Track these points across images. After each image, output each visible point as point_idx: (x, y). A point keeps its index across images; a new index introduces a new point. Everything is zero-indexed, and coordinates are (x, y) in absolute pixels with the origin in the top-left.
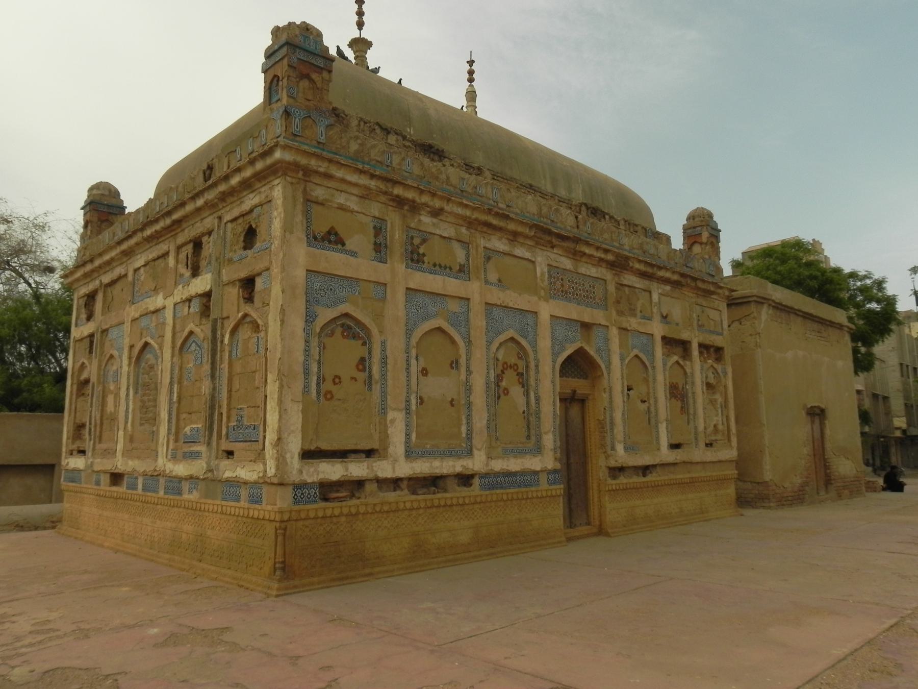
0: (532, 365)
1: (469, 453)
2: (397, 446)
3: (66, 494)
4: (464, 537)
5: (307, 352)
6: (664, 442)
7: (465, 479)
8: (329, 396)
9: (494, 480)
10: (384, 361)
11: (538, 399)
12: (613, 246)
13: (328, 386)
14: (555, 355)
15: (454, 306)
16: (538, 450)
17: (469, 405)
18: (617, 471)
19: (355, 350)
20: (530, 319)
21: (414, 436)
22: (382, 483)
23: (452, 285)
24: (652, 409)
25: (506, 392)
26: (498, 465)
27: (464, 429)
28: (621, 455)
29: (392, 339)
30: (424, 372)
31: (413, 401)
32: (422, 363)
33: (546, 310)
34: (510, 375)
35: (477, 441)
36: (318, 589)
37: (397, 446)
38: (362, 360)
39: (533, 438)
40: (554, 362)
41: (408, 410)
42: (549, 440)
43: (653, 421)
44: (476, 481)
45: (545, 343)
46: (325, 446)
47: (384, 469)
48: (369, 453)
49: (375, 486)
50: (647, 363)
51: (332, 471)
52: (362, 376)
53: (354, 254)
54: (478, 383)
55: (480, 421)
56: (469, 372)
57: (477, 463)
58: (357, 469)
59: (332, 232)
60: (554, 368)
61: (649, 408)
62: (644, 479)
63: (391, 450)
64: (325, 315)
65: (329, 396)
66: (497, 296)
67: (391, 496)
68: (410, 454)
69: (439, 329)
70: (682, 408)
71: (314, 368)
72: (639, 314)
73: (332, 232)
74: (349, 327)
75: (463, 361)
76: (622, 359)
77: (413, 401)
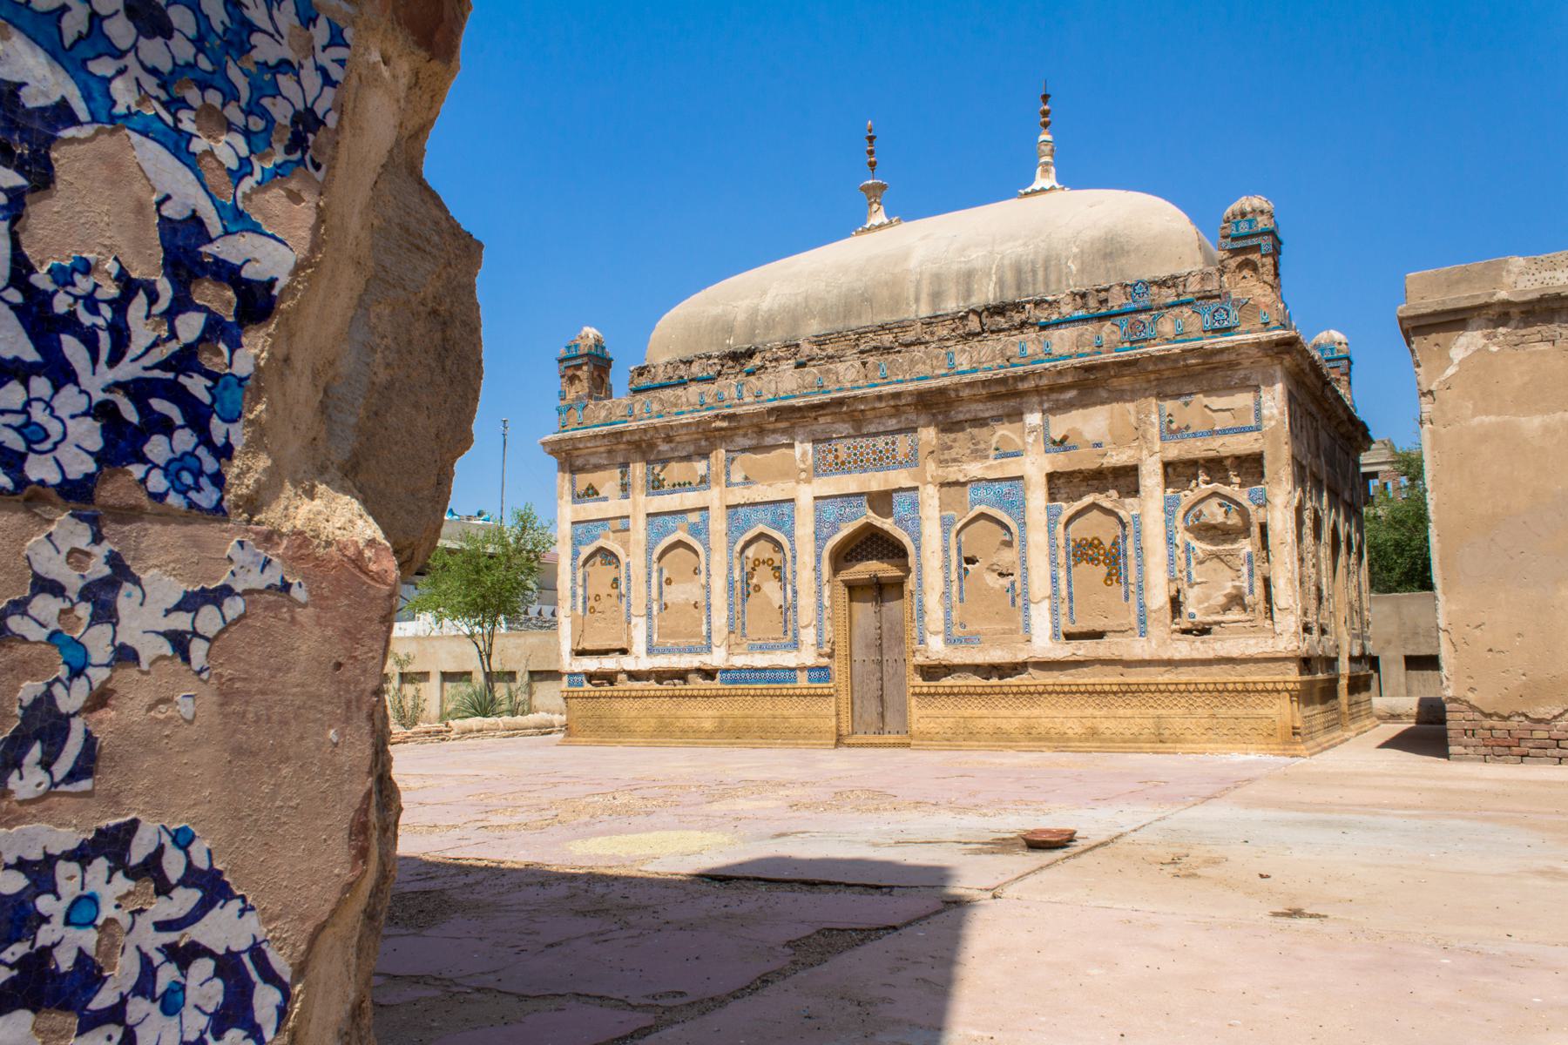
0: (789, 556)
1: (709, 649)
2: (639, 646)
3: (83, 678)
4: (708, 725)
5: (574, 580)
6: (566, 646)
7: (709, 674)
8: (593, 610)
9: (737, 675)
10: (629, 578)
11: (795, 592)
12: (938, 377)
13: (591, 603)
14: (819, 538)
15: (694, 518)
16: (795, 645)
17: (709, 607)
18: (931, 672)
19: (609, 572)
20: (786, 508)
21: (655, 637)
22: (633, 676)
23: (690, 499)
24: (1018, 585)
25: (758, 588)
26: (739, 661)
27: (704, 628)
28: (937, 649)
29: (634, 558)
30: (669, 582)
31: (655, 607)
32: (666, 574)
33: (805, 495)
34: (765, 571)
35: (716, 640)
36: (894, 745)
37: (639, 646)
38: (616, 580)
39: (790, 633)
40: (820, 548)
41: (649, 615)
42: (808, 636)
43: (1019, 602)
44: (565, 678)
45: (805, 528)
46: (588, 646)
47: (628, 663)
48: (624, 652)
49: (624, 676)
50: (1006, 519)
51: (591, 664)
52: (614, 592)
53: (605, 499)
54: (719, 585)
55: (720, 618)
56: (709, 575)
57: (716, 659)
58: (609, 664)
59: (591, 487)
60: (818, 558)
61: (1013, 584)
62: (984, 682)
63: (634, 649)
64: (586, 551)
65: (593, 610)
66: (739, 495)
67: (638, 685)
68: (650, 651)
69: (982, 516)
70: (1109, 574)
71: (580, 591)
72: (992, 453)
73: (591, 487)
74: (607, 555)
75: (703, 567)
76: (946, 524)
77: (655, 607)
